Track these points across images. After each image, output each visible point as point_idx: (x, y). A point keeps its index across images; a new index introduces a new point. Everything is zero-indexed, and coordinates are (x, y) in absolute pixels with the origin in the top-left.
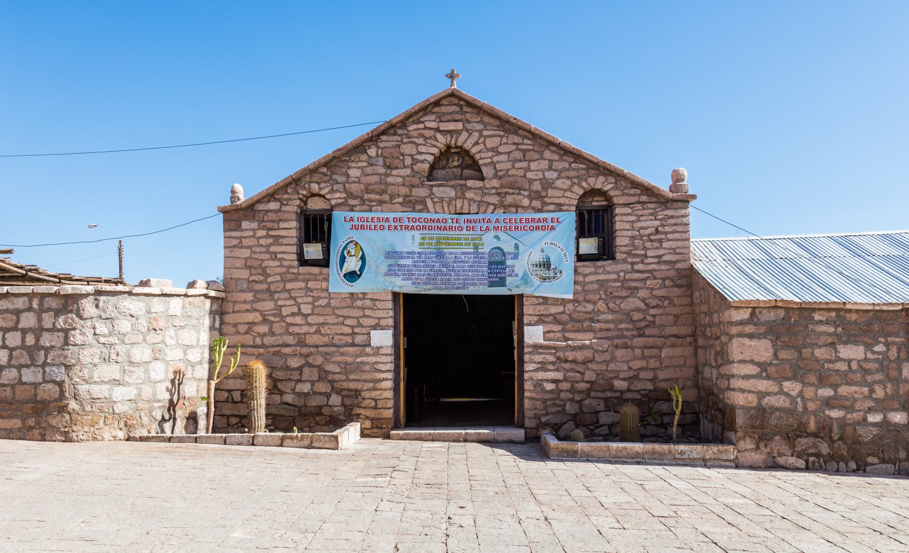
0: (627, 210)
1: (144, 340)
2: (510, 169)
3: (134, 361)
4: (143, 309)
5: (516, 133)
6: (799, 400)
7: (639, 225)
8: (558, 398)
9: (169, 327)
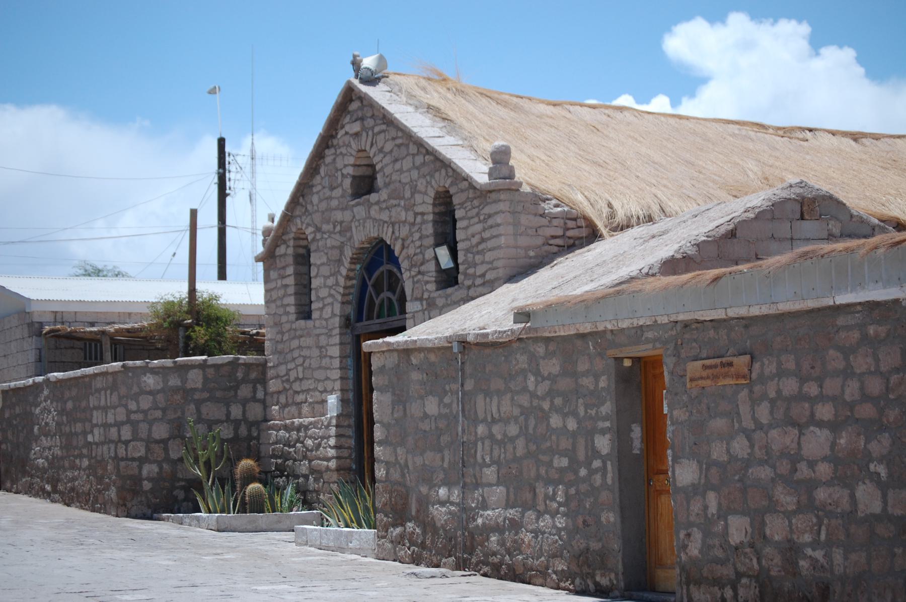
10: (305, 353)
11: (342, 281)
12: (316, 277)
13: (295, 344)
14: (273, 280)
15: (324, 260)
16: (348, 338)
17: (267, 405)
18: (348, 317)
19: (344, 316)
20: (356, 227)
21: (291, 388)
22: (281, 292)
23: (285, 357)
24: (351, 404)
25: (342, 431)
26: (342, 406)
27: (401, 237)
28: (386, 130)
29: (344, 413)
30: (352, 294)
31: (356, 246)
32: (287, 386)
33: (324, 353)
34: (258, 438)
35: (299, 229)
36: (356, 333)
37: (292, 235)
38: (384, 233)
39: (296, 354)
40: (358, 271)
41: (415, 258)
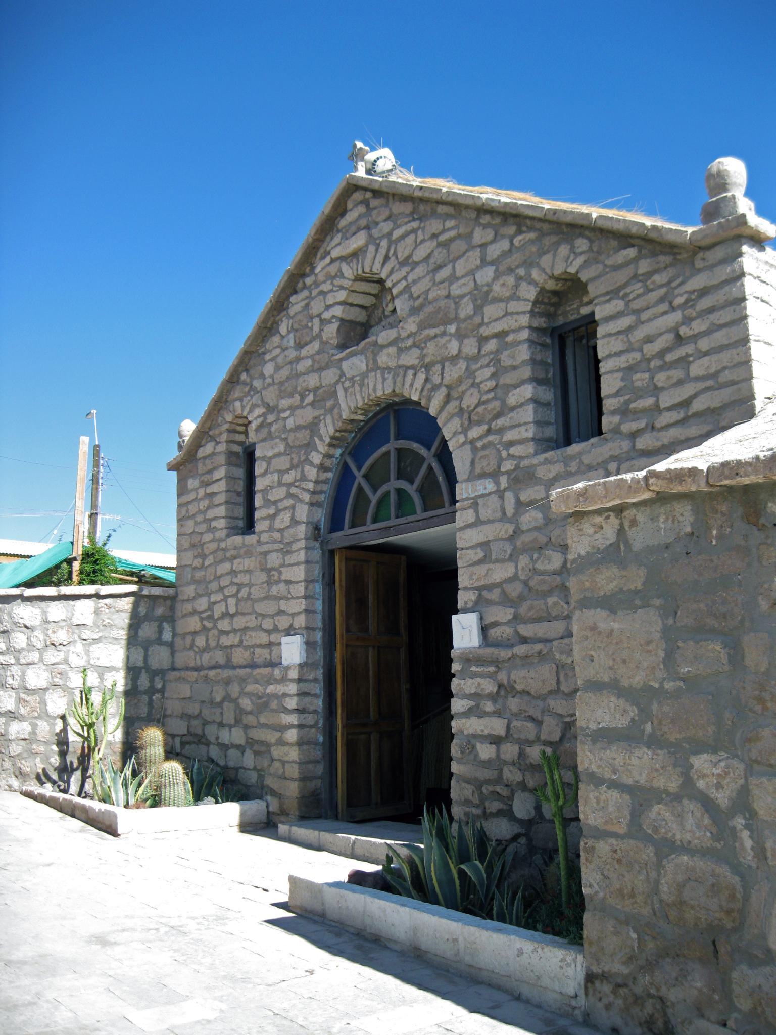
0: (617, 305)
1: (41, 660)
2: (429, 289)
3: (29, 687)
4: (39, 617)
5: (434, 213)
6: (739, 822)
7: (639, 334)
8: (499, 780)
9: (75, 641)
10: (242, 579)
11: (312, 473)
12: (264, 474)
13: (226, 566)
14: (192, 490)
15: (281, 448)
16: (317, 555)
17: (176, 649)
18: (317, 525)
19: (312, 523)
20: (346, 390)
21: (215, 627)
22: (204, 504)
23: (207, 587)
24: (318, 648)
25: (306, 687)
26: (307, 651)
27: (445, 382)
28: (419, 228)
29: (310, 661)
30: (325, 492)
31: (344, 417)
32: (209, 625)
33: (276, 578)
34: (162, 691)
35: (237, 417)
36: (330, 547)
37: (226, 426)
38: (407, 386)
39: (225, 581)
40: (337, 458)
41: (480, 409)
